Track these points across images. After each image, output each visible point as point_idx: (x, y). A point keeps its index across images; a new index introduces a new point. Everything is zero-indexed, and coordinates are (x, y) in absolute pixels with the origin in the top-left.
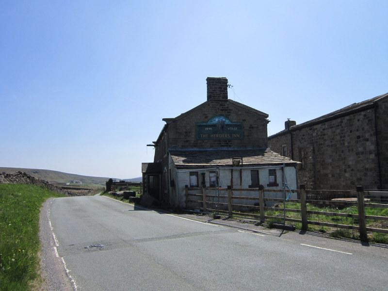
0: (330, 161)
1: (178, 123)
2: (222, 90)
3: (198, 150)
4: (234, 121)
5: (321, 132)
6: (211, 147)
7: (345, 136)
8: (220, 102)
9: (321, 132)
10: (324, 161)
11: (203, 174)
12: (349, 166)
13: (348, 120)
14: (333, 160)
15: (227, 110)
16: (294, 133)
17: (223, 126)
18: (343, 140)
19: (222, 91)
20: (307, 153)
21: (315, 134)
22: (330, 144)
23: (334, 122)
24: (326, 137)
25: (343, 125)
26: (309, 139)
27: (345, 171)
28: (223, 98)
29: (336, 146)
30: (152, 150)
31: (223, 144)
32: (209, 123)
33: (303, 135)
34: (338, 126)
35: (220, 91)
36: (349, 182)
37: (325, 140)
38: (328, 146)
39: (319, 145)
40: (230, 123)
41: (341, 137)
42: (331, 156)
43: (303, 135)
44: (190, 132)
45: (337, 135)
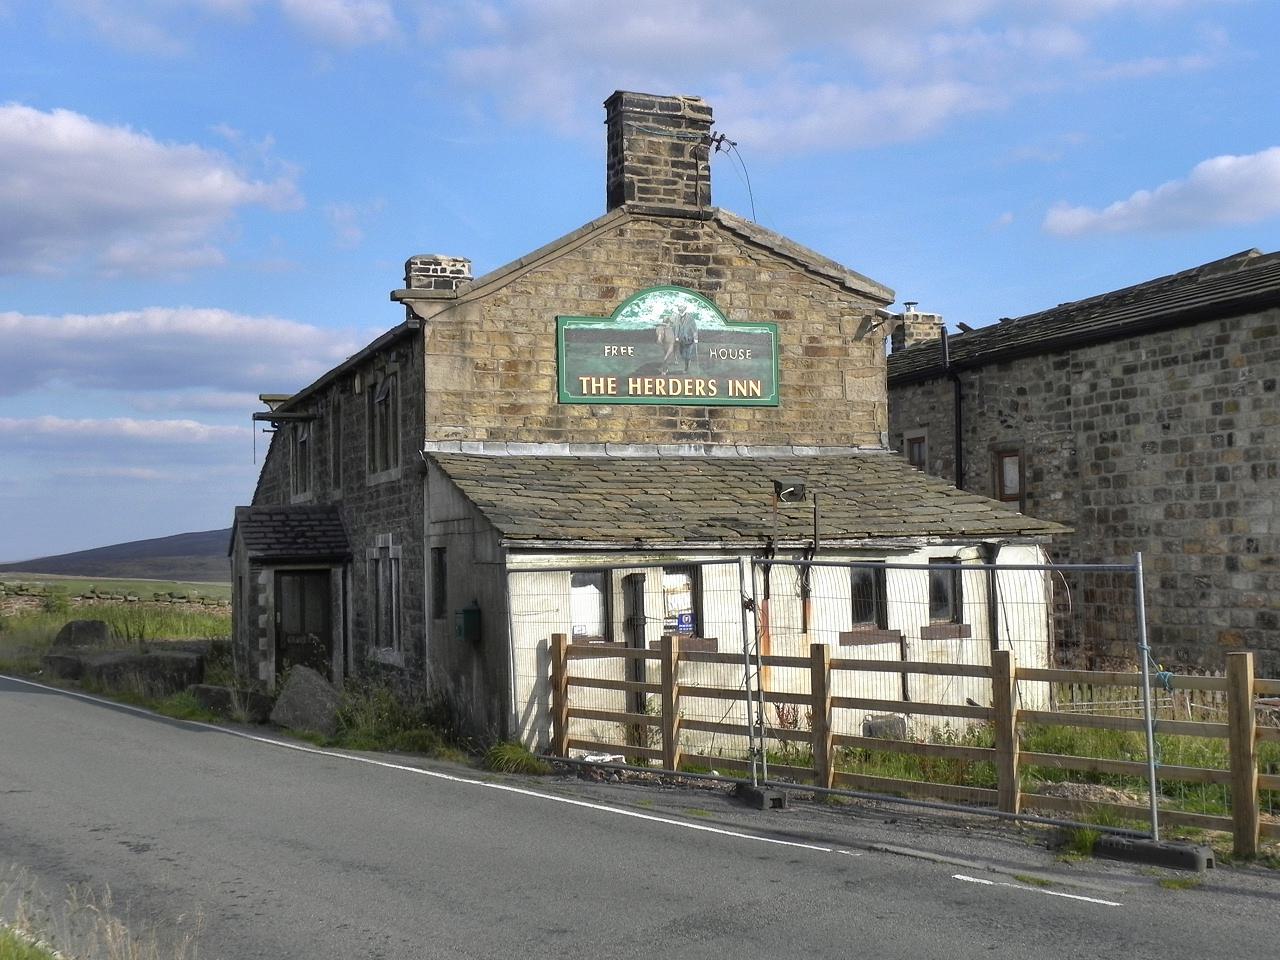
0: (1157, 514)
1: (474, 316)
2: (687, 158)
3: (566, 452)
4: (737, 315)
5: (1116, 382)
6: (629, 440)
7: (1236, 407)
8: (675, 221)
9: (1116, 382)
10: (1122, 514)
11: (634, 585)
12: (1252, 546)
13: (1259, 333)
14: (1169, 513)
15: (705, 262)
16: (974, 377)
17: (687, 345)
18: (1228, 424)
19: (688, 166)
20: (1038, 476)
21: (1080, 389)
22: (1158, 437)
23: (1183, 336)
24: (1138, 405)
25: (1232, 351)
26: (1050, 408)
27: (1232, 565)
28: (691, 198)
29: (1191, 447)
30: (264, 433)
31: (685, 428)
32: (623, 323)
33: (1022, 392)
34: (1205, 356)
35: (675, 164)
36: (1251, 615)
37: (1135, 419)
38: (1149, 447)
39: (1103, 440)
40: (718, 325)
41: (1217, 408)
42: (1159, 494)
43: (1022, 392)
44: (529, 364)
45: (1195, 398)
